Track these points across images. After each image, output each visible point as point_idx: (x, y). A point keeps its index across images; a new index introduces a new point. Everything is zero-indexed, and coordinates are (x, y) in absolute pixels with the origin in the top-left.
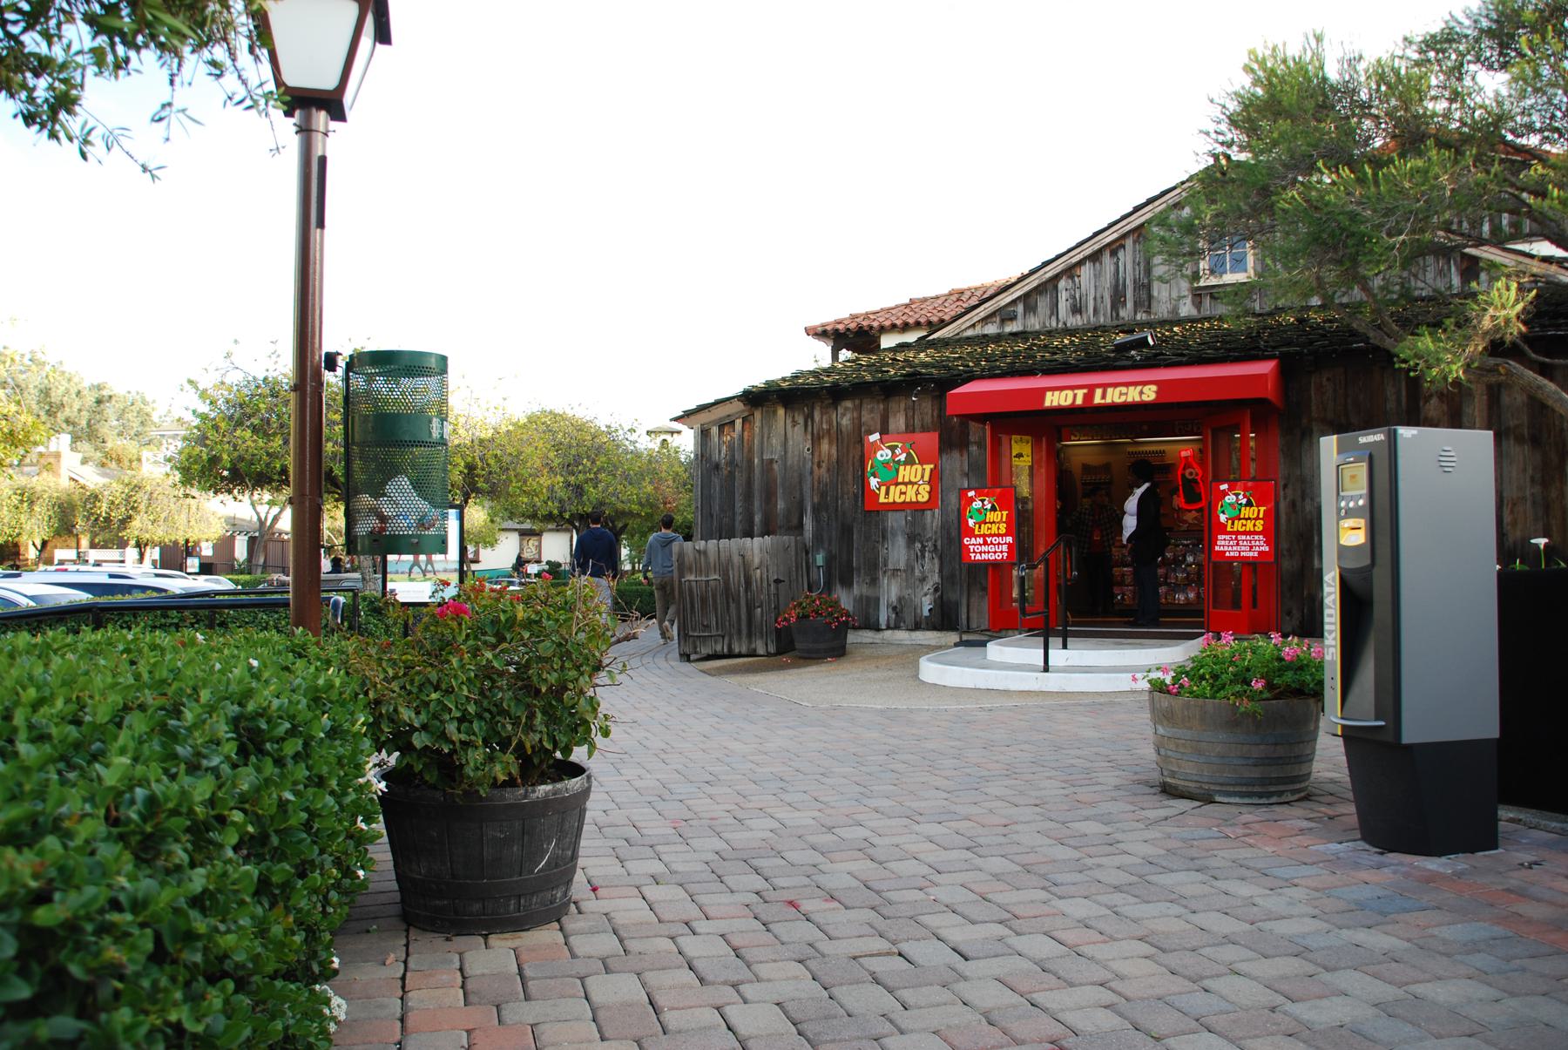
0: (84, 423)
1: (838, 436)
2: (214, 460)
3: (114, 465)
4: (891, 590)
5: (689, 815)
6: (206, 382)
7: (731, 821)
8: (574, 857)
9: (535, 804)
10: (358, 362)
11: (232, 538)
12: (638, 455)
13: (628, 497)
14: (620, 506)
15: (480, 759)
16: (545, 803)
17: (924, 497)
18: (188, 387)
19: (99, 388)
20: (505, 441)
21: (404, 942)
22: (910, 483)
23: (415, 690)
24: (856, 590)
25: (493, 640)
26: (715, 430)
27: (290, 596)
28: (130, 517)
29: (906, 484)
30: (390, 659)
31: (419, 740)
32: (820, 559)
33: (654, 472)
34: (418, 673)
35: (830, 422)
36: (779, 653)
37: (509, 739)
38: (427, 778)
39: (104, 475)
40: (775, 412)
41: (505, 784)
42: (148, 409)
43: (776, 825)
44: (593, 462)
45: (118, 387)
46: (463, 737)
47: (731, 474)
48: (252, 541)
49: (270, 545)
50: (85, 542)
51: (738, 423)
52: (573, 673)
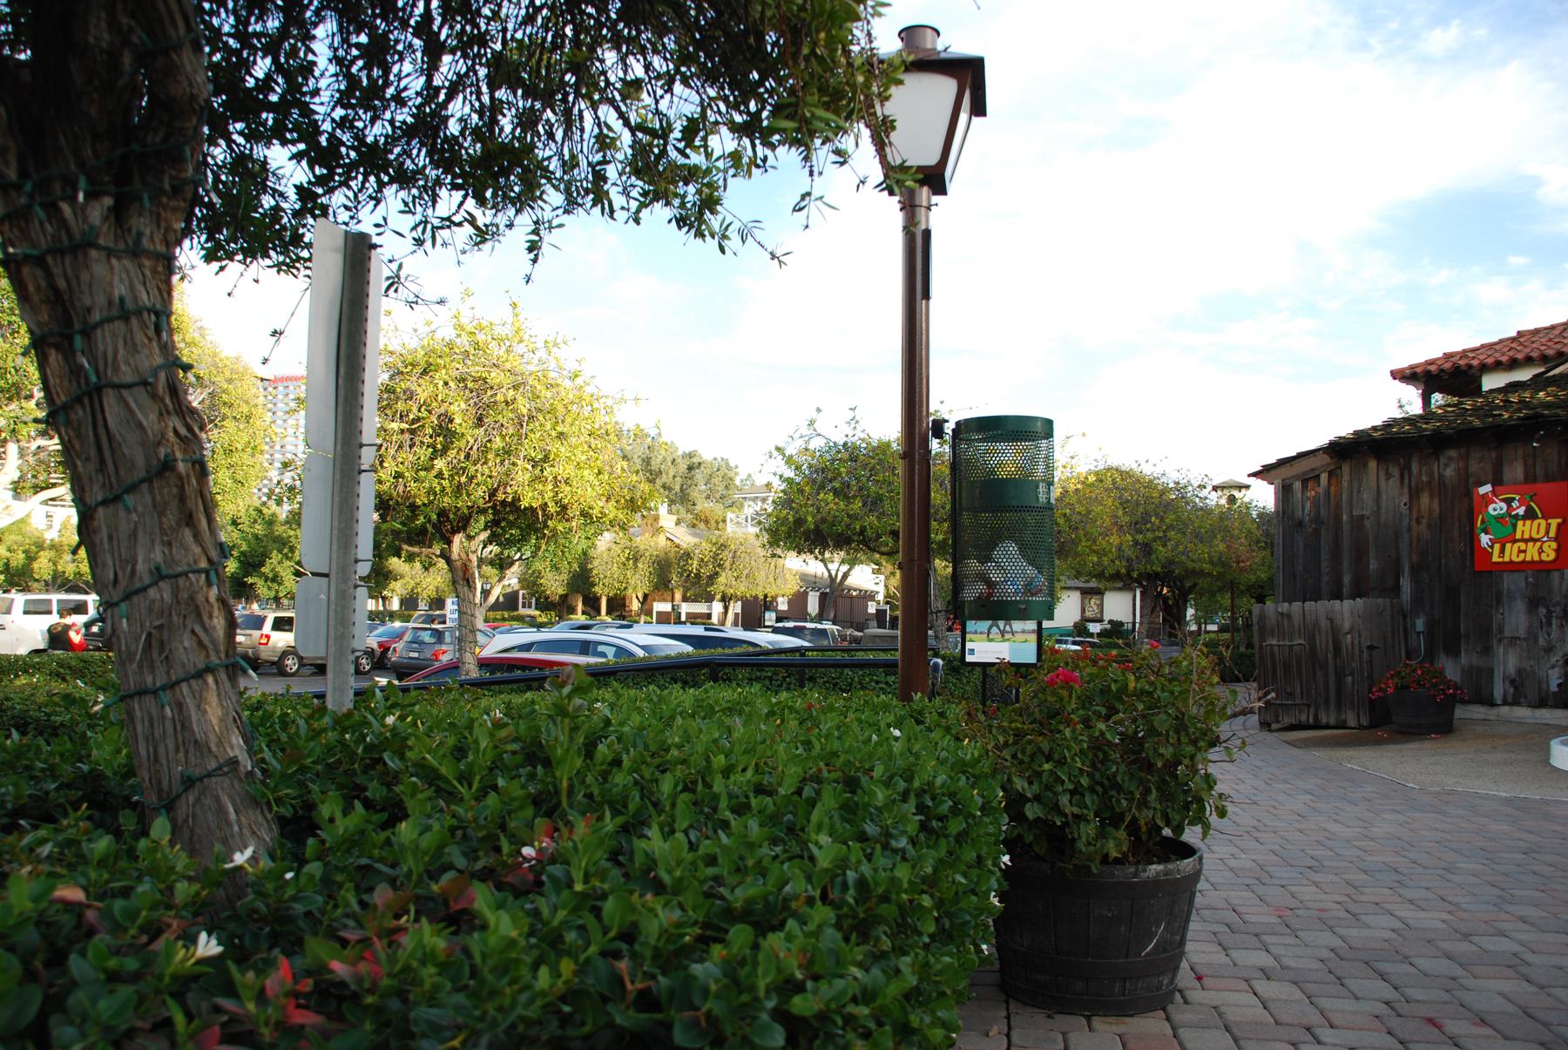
0: (677, 488)
1: (1439, 488)
2: (799, 522)
3: (702, 525)
4: (1508, 662)
5: (1294, 903)
6: (791, 450)
7: (1343, 914)
8: (1182, 943)
9: (1145, 883)
10: (963, 427)
11: (805, 594)
12: (1207, 511)
13: (1201, 555)
14: (1190, 565)
15: (1092, 833)
16: (1156, 883)
17: (1549, 554)
18: (775, 453)
19: (691, 455)
20: (1074, 500)
21: (1004, 1014)
22: (1535, 540)
23: (1026, 759)
24: (1464, 660)
25: (1103, 711)
26: (1297, 485)
27: (898, 656)
28: (717, 573)
29: (1526, 541)
30: (1000, 727)
31: (1031, 811)
32: (1420, 624)
33: (1227, 530)
34: (1030, 742)
35: (1430, 474)
36: (1373, 725)
37: (1122, 816)
38: (1037, 849)
39: (695, 535)
40: (1365, 465)
41: (1117, 861)
42: (731, 474)
43: (1399, 925)
44: (1162, 519)
45: (707, 455)
46: (1076, 810)
47: (1317, 532)
48: (823, 598)
49: (840, 601)
50: (678, 596)
51: (1324, 477)
52: (1190, 749)
